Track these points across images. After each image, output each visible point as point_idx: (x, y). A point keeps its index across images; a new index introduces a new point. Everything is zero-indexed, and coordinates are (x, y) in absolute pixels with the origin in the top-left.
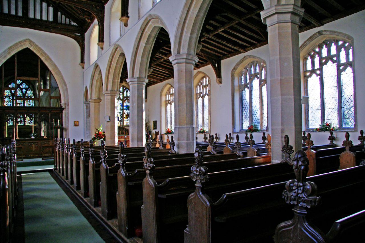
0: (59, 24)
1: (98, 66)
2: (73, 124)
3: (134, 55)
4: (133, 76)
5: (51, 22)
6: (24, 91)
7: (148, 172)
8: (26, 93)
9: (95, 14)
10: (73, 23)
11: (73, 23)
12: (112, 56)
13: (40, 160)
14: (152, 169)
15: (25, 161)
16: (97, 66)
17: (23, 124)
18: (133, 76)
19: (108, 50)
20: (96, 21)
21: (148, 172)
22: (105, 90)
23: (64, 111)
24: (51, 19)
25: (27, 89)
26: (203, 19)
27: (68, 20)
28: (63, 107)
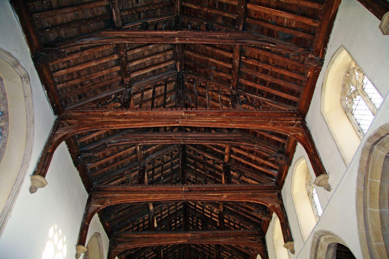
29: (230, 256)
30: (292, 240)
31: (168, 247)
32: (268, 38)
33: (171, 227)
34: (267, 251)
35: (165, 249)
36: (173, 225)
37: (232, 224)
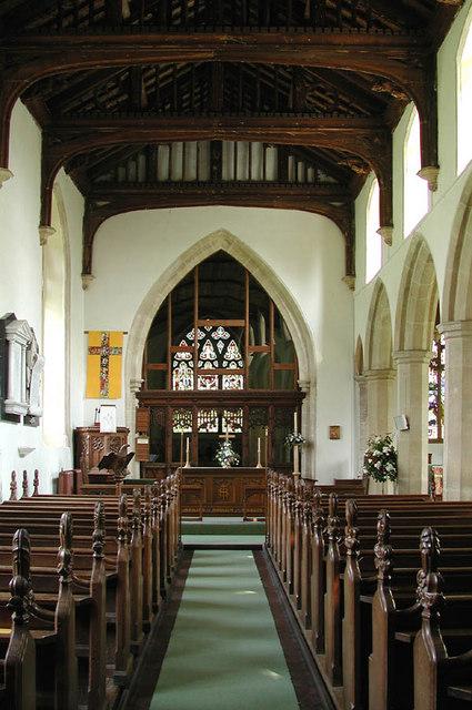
1: (382, 284)
2: (326, 433)
3: (451, 264)
4: (451, 319)
6: (220, 346)
7: (426, 614)
8: (225, 350)
9: (368, 159)
10: (322, 177)
12: (409, 263)
13: (238, 520)
14: (437, 605)
15: (208, 521)
16: (380, 288)
17: (215, 430)
18: (451, 319)
21: (426, 614)
23: (304, 401)
24: (270, 175)
25: (226, 342)
27: (310, 171)
28: (304, 390)
29: (330, 104)
30: (354, 275)
31: (160, 76)
32: (73, 663)
33: (170, 19)
34: (436, 93)
35: (153, 81)
36: (175, 12)
37: (348, 14)
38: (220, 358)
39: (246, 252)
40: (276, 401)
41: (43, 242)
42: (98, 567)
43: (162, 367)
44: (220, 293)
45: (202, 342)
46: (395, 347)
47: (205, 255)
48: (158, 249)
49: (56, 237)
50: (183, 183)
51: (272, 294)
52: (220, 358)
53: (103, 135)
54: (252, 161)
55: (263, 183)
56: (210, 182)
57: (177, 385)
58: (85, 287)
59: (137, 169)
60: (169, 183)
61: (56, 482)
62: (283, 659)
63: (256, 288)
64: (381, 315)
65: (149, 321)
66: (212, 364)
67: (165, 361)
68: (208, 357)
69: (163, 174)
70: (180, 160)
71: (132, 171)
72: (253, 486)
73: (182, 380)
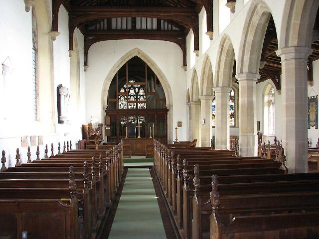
0: (162, 31)
5: (154, 30)
6: (137, 90)
8: (139, 92)
10: (174, 28)
11: (174, 28)
13: (144, 157)
16: (195, 71)
19: (202, 60)
20: (191, 30)
22: (240, 72)
25: (139, 89)
26: (261, 42)
27: (170, 26)
38: (137, 94)
39: (145, 57)
40: (158, 113)
41: (70, 56)
42: (73, 197)
43: (114, 100)
44: (136, 71)
45: (130, 89)
46: (200, 94)
47: (130, 58)
48: (112, 56)
49: (74, 52)
50: (122, 30)
51: (156, 73)
52: (137, 94)
53: (91, 15)
54: (148, 23)
55: (152, 30)
56: (132, 30)
57: (120, 105)
58: (85, 70)
59: (104, 25)
60: (116, 30)
61: (76, 144)
62: (164, 230)
63: (149, 68)
64: (195, 82)
65: (109, 83)
66: (134, 98)
67: (116, 98)
68: (132, 94)
69: (114, 27)
70: (120, 22)
71: (102, 25)
72: (149, 144)
73: (122, 104)
